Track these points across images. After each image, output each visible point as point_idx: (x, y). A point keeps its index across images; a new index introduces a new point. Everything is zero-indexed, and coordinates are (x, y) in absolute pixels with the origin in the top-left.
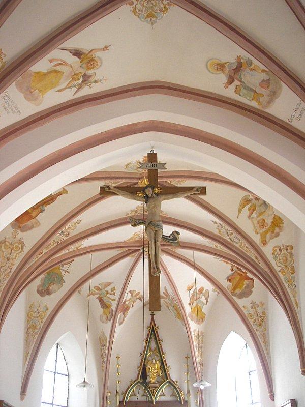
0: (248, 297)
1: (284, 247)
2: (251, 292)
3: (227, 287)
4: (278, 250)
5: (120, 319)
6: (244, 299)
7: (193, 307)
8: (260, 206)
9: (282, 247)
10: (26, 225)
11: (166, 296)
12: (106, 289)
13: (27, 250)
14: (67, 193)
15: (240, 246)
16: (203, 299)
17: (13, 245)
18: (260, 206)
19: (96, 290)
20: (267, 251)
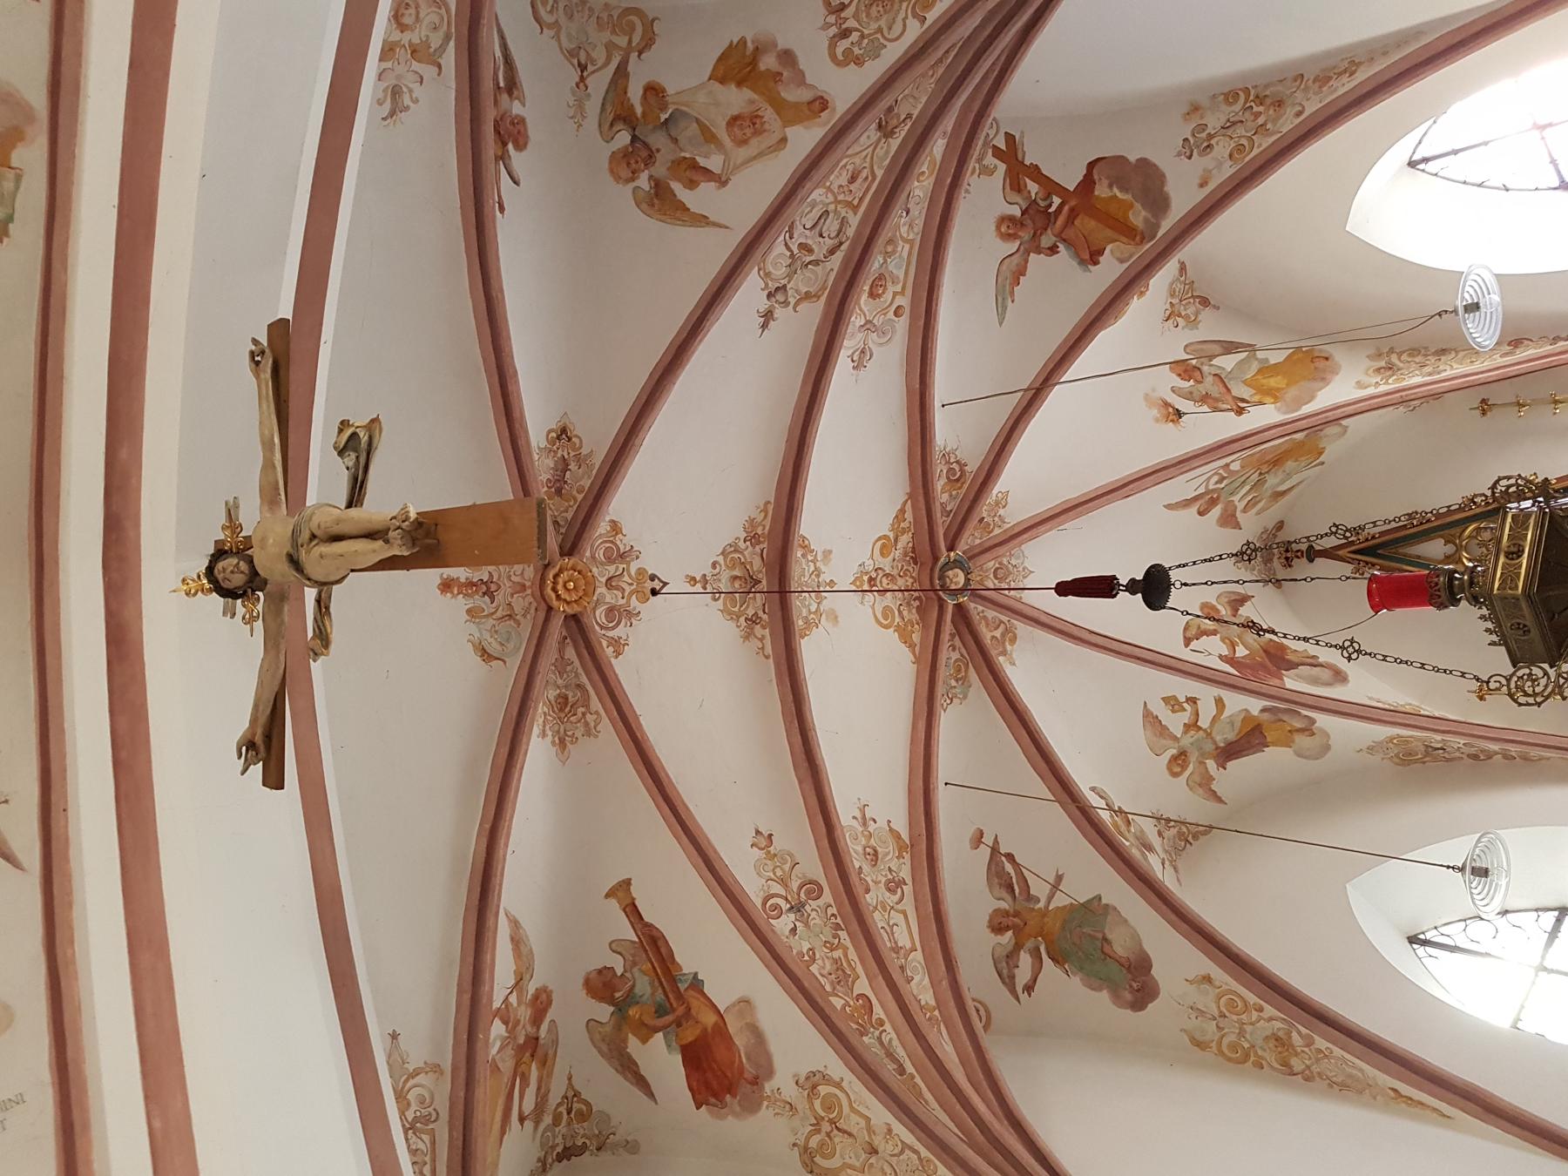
0: (1163, 175)
1: (832, 19)
2: (1144, 163)
3: (1122, 261)
4: (843, 45)
5: (1315, 681)
6: (1171, 188)
7: (1256, 398)
8: (675, 141)
9: (833, 30)
10: (748, 1059)
11: (1213, 502)
12: (1178, 732)
13: (836, 1067)
14: (628, 882)
15: (855, 209)
16: (1227, 362)
17: (819, 1119)
18: (675, 141)
19: (1184, 768)
20: (846, 87)
